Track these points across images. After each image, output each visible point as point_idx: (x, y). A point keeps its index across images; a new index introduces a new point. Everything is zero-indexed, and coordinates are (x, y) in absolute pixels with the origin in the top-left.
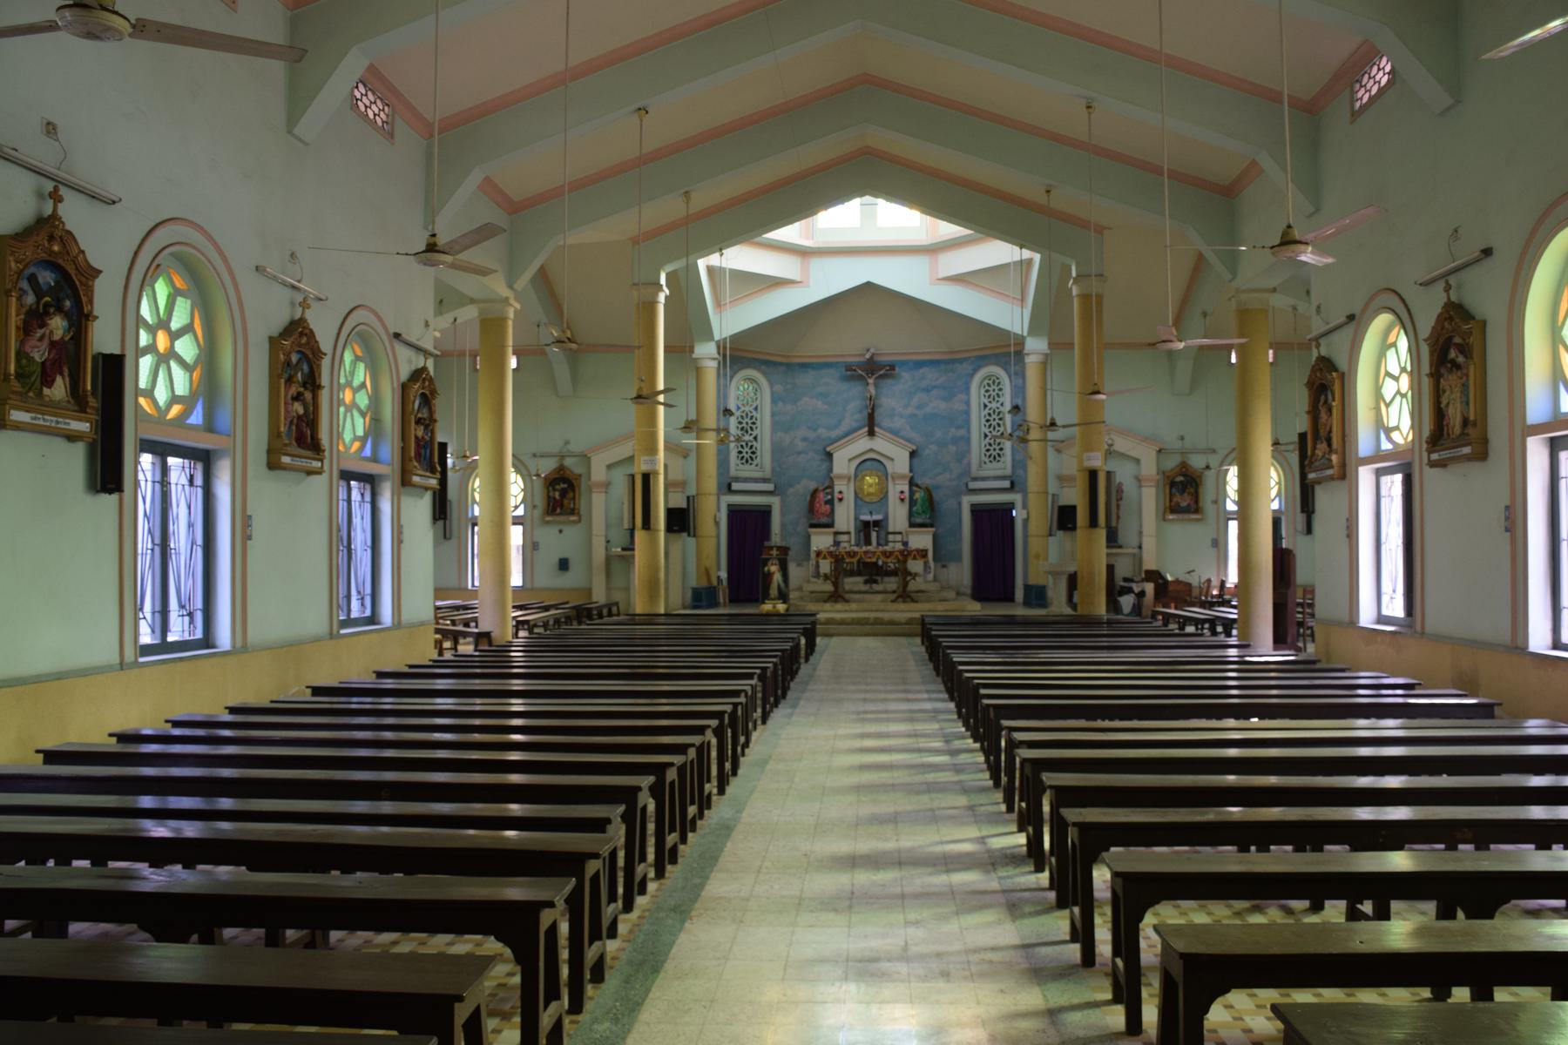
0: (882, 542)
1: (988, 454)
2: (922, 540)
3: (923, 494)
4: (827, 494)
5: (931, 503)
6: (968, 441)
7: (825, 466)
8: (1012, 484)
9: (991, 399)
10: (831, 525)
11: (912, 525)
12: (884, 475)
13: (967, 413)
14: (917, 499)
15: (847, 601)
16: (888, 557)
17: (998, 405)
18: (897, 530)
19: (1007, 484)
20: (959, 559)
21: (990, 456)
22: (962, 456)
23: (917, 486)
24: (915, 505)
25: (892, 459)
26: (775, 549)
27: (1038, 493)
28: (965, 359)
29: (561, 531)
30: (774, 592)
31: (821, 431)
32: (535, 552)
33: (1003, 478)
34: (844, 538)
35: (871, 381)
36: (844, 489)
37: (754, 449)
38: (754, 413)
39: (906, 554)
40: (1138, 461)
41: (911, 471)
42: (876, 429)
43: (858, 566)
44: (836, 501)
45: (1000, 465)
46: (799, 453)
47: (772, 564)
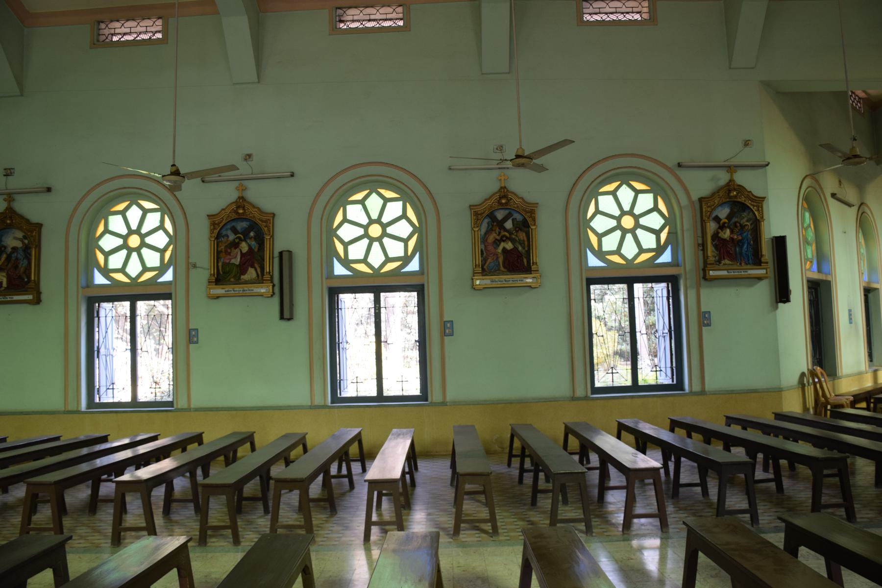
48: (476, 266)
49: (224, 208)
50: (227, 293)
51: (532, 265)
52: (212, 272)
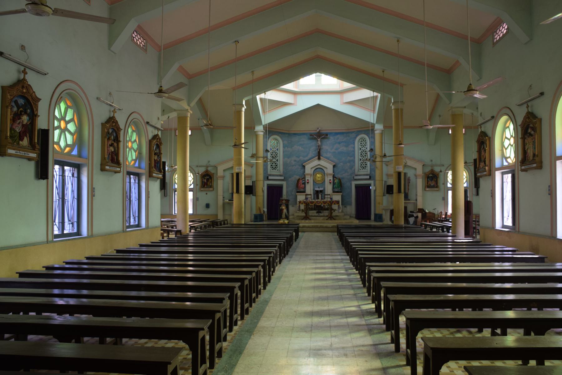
0: (323, 198)
1: (361, 166)
2: (337, 197)
3: (338, 180)
4: (303, 180)
5: (341, 184)
6: (354, 161)
7: (302, 170)
8: (370, 177)
9: (362, 146)
10: (304, 192)
11: (334, 192)
12: (324, 174)
13: (354, 151)
14: (336, 183)
15: (310, 219)
16: (325, 204)
17: (365, 149)
18: (328, 194)
19: (368, 177)
20: (351, 204)
21: (362, 167)
22: (352, 167)
23: (336, 178)
24: (335, 185)
25: (327, 168)
26: (284, 201)
27: (380, 180)
28: (353, 132)
29: (207, 194)
30: (284, 216)
31: (301, 158)
33: (367, 175)
34: (309, 196)
35: (319, 140)
36: (309, 179)
37: (276, 164)
38: (277, 151)
39: (332, 202)
40: (416, 169)
41: (333, 172)
42: (321, 157)
43: (314, 207)
44: (306, 183)
45: (366, 170)
46: (293, 166)
47: (283, 206)
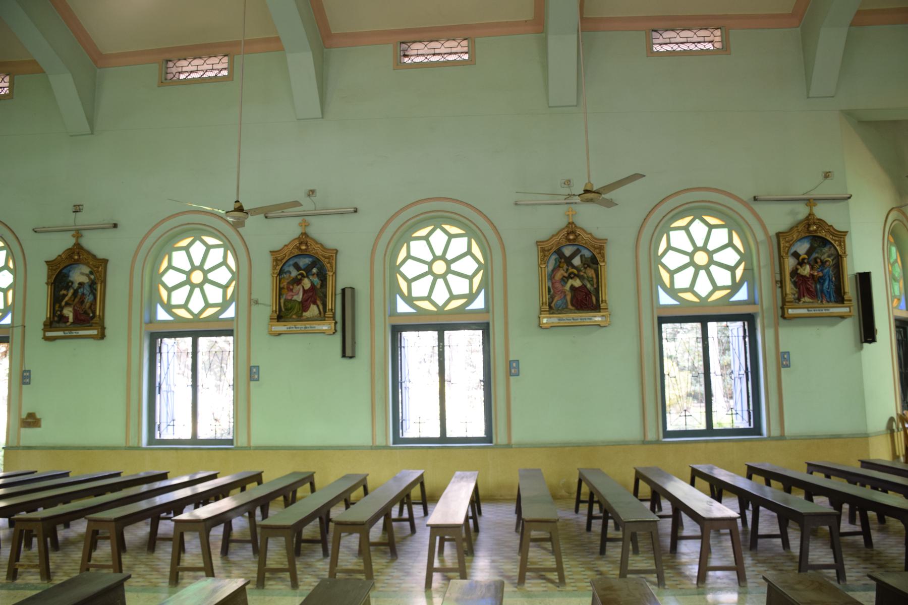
32: (24, 387)
48: (543, 303)
49: (287, 244)
50: (289, 330)
51: (601, 302)
52: (274, 309)
